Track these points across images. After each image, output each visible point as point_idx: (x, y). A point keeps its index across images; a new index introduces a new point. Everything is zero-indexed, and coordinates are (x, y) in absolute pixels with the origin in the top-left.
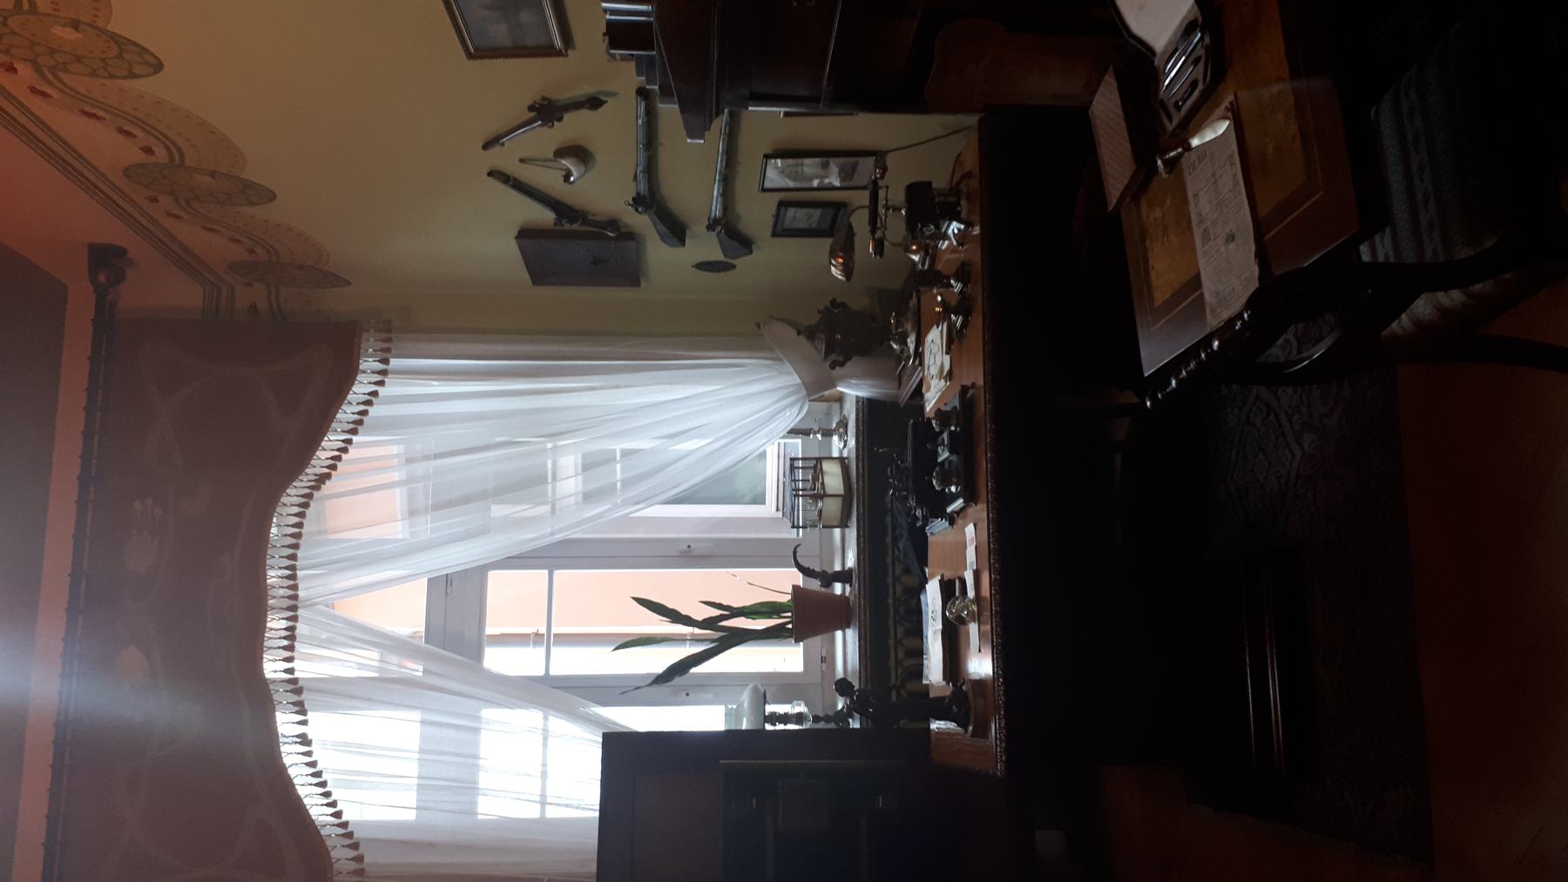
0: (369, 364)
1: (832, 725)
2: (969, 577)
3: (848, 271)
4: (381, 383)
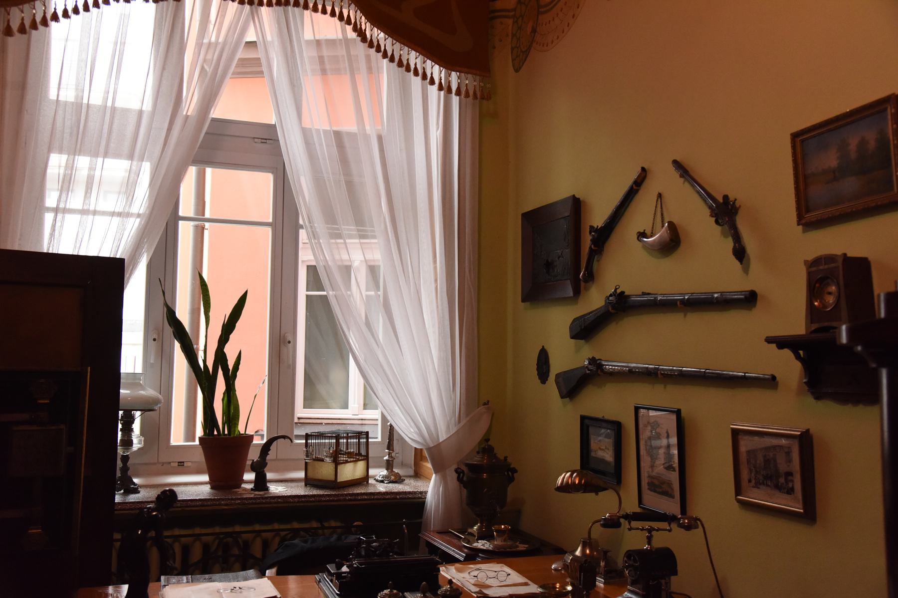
1: (118, 474)
3: (566, 488)
4: (441, 88)
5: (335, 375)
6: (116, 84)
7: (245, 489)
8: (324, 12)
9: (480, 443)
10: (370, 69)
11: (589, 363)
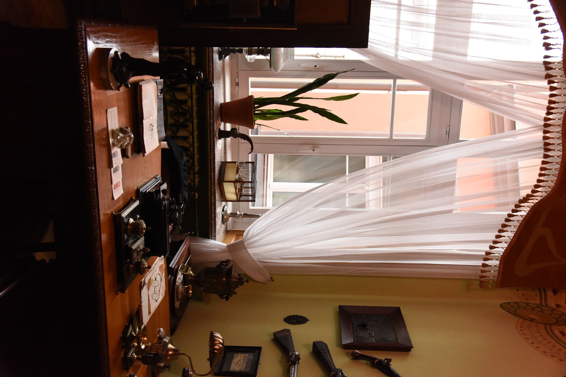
0: (494, 263)
2: (118, 160)
3: (212, 338)
5: (295, 174)
6: (483, 39)
7: (220, 124)
8: (540, 175)
9: (246, 275)
10: (499, 205)
11: (296, 356)
